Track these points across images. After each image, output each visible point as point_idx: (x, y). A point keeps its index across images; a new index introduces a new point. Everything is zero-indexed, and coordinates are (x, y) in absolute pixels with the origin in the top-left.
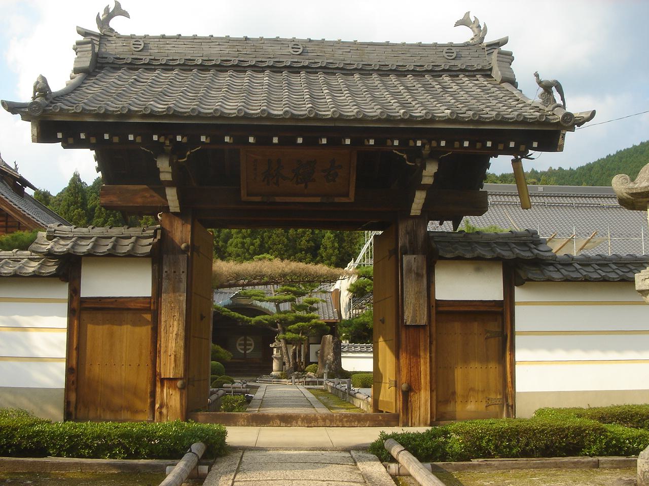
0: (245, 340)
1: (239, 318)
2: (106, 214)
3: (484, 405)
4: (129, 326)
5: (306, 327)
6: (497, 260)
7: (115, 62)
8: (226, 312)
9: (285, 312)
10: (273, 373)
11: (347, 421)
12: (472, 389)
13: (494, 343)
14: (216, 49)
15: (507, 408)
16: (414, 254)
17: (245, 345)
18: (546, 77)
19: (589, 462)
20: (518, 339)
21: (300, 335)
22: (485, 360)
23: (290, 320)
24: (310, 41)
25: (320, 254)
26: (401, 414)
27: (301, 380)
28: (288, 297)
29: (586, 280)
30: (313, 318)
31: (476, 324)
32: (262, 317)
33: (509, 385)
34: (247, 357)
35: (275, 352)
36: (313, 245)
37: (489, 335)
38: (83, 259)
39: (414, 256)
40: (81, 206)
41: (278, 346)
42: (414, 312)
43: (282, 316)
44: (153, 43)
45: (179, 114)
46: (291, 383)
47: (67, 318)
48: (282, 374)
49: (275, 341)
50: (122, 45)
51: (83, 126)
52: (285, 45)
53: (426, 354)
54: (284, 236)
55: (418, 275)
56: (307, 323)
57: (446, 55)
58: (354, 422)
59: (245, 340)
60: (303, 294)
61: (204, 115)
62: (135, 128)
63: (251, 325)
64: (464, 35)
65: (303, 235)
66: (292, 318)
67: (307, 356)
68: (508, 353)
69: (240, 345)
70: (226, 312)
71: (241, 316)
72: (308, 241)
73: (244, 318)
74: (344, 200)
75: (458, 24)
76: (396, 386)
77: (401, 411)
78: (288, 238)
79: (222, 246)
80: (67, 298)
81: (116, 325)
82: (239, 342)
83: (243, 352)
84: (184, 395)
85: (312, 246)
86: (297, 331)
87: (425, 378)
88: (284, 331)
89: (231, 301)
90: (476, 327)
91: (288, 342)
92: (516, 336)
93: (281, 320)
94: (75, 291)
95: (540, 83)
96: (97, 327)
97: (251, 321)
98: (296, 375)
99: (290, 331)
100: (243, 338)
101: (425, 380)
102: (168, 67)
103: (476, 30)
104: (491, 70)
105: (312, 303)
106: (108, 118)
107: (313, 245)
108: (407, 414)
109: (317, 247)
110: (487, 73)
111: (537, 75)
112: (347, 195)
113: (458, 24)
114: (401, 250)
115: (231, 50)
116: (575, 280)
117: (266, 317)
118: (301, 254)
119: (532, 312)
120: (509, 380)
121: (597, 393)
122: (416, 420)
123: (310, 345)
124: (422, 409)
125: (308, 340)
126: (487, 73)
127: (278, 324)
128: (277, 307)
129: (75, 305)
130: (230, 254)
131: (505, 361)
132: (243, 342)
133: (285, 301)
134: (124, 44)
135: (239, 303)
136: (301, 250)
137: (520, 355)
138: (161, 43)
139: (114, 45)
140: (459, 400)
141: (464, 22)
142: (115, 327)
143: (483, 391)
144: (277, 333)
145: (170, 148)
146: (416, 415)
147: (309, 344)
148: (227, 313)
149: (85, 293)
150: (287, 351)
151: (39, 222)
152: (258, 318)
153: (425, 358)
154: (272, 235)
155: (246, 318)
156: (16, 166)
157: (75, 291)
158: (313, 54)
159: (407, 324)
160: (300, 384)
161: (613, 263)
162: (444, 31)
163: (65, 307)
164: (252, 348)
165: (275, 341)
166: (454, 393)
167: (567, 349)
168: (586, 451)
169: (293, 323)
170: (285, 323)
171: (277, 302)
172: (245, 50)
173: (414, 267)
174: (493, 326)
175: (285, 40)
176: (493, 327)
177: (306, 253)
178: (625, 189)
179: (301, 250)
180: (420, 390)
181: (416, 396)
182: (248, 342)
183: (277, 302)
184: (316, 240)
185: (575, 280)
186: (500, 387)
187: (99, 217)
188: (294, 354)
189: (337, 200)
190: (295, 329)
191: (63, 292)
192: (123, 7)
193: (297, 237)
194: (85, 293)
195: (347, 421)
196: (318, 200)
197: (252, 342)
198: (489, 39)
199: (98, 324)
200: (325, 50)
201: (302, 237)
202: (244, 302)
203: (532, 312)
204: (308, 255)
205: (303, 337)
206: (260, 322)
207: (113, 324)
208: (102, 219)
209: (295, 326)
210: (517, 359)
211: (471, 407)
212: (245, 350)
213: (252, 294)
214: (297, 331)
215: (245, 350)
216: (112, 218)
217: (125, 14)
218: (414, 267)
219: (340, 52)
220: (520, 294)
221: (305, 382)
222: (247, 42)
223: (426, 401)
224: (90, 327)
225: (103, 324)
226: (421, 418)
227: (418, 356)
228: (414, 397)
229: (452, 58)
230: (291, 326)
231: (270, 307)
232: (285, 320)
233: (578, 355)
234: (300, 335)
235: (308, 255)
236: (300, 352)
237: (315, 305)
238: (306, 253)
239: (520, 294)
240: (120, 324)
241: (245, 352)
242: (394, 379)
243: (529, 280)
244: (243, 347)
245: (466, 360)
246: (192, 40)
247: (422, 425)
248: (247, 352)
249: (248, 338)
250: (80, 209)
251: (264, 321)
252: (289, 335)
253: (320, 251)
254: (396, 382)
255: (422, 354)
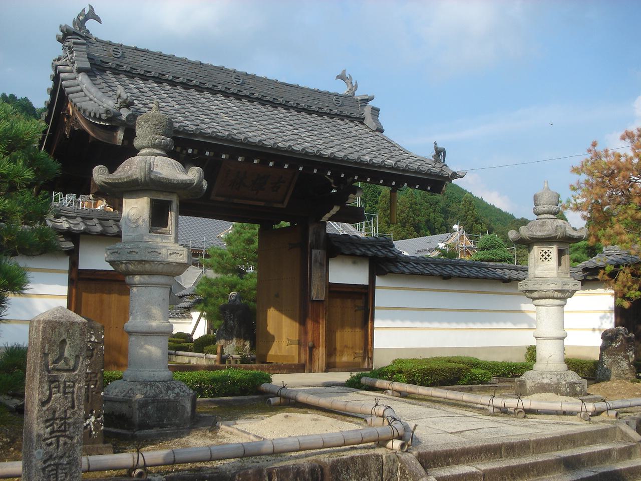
3: (353, 357)
4: (116, 295)
6: (363, 256)
7: (102, 65)
11: (272, 370)
12: (346, 346)
13: (359, 314)
14: (179, 68)
15: (368, 359)
16: (318, 249)
18: (439, 146)
19: (468, 388)
20: (376, 312)
22: (353, 326)
24: (247, 74)
26: (308, 364)
29: (485, 278)
31: (349, 301)
33: (370, 343)
37: (356, 308)
38: (81, 236)
39: (319, 251)
42: (317, 292)
44: (128, 52)
45: (234, 140)
47: (67, 287)
50: (102, 49)
51: (201, 147)
52: (229, 75)
53: (323, 321)
55: (321, 264)
57: (335, 102)
58: (277, 370)
61: (250, 144)
62: (224, 149)
64: (342, 89)
68: (370, 321)
74: (280, 206)
75: (339, 77)
76: (299, 344)
77: (308, 361)
80: (68, 269)
81: (106, 294)
87: (323, 338)
90: (349, 303)
92: (375, 310)
94: (74, 264)
95: (436, 149)
96: (90, 295)
101: (322, 340)
102: (131, 75)
103: (350, 86)
104: (364, 119)
106: (179, 135)
108: (311, 364)
110: (361, 120)
111: (435, 144)
112: (282, 202)
113: (339, 77)
114: (310, 246)
115: (190, 71)
116: (415, 274)
119: (386, 294)
120: (370, 340)
121: (418, 350)
122: (316, 368)
124: (320, 361)
126: (361, 120)
129: (74, 275)
131: (368, 327)
134: (104, 49)
137: (377, 323)
138: (135, 54)
139: (96, 48)
140: (338, 353)
141: (342, 77)
142: (105, 296)
143: (352, 348)
145: (184, 156)
146: (317, 364)
149: (82, 266)
153: (323, 324)
157: (74, 264)
158: (249, 86)
159: (314, 299)
161: (431, 263)
162: (321, 79)
163: (65, 277)
166: (335, 349)
167: (403, 319)
168: (461, 382)
172: (200, 73)
173: (319, 259)
174: (361, 303)
175: (228, 70)
176: (360, 303)
178: (529, 235)
180: (319, 346)
181: (317, 351)
185: (415, 274)
186: (362, 345)
189: (275, 205)
191: (65, 264)
192: (96, 12)
194: (82, 266)
195: (272, 370)
196: (262, 204)
198: (359, 94)
199: (91, 293)
200: (257, 83)
203: (386, 294)
207: (103, 292)
210: (375, 325)
211: (345, 359)
217: (98, 19)
218: (319, 259)
219: (267, 87)
220: (379, 282)
222: (201, 66)
223: (322, 355)
224: (84, 295)
225: (95, 293)
226: (320, 366)
227: (319, 323)
228: (315, 352)
229: (339, 105)
233: (408, 324)
239: (379, 282)
240: (110, 293)
242: (297, 338)
243: (391, 272)
245: (343, 326)
246: (160, 57)
247: (320, 371)
254: (299, 341)
255: (321, 321)
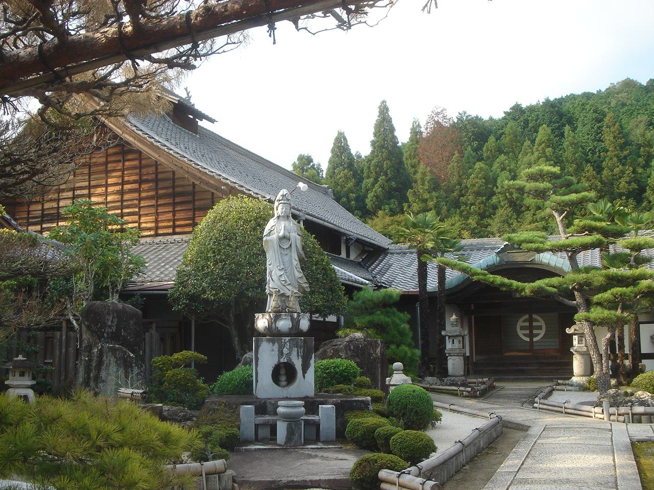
0: (531, 320)
1: (503, 285)
2: (376, 172)
5: (629, 296)
8: (478, 274)
9: (587, 270)
10: (574, 379)
17: (531, 328)
21: (619, 312)
23: (596, 284)
25: (646, 198)
27: (622, 410)
28: (588, 239)
30: (643, 277)
32: (547, 280)
34: (535, 348)
35: (575, 342)
36: (636, 187)
40: (348, 167)
41: (581, 331)
43: (582, 277)
46: (601, 416)
48: (590, 382)
49: (575, 323)
54: (596, 178)
56: (630, 289)
59: (531, 320)
60: (620, 234)
63: (526, 298)
65: (621, 175)
66: (601, 279)
67: (636, 345)
69: (522, 328)
70: (478, 274)
71: (506, 280)
72: (629, 183)
73: (511, 285)
78: (601, 181)
79: (517, 198)
82: (520, 323)
83: (528, 339)
84: (503, 377)
85: (635, 188)
86: (612, 305)
88: (588, 304)
89: (498, 258)
91: (593, 323)
93: (579, 284)
97: (523, 289)
98: (613, 396)
99: (599, 304)
100: (527, 316)
105: (637, 248)
107: (636, 187)
109: (642, 190)
117: (555, 280)
118: (621, 199)
123: (640, 325)
125: (637, 318)
127: (576, 293)
128: (572, 259)
130: (528, 207)
132: (527, 324)
133: (585, 247)
135: (511, 260)
136: (620, 195)
144: (575, 310)
147: (638, 324)
148: (481, 277)
150: (595, 341)
151: (171, 152)
152: (539, 283)
154: (581, 179)
155: (515, 283)
156: (188, 94)
160: (621, 418)
164: (542, 333)
165: (575, 323)
169: (603, 289)
170: (587, 290)
171: (573, 251)
177: (627, 198)
179: (620, 195)
182: (535, 324)
183: (573, 251)
184: (639, 181)
187: (368, 177)
188: (611, 343)
190: (609, 301)
193: (614, 179)
197: (542, 323)
201: (620, 178)
202: (519, 257)
204: (631, 201)
205: (625, 314)
206: (540, 291)
208: (372, 179)
209: (607, 295)
212: (531, 336)
213: (522, 239)
214: (612, 305)
215: (531, 336)
216: (384, 177)
221: (633, 414)
230: (600, 295)
231: (559, 261)
232: (588, 283)
234: (619, 312)
235: (631, 201)
236: (621, 339)
237: (644, 253)
238: (627, 198)
241: (531, 340)
244: (527, 332)
248: (535, 339)
249: (534, 316)
250: (346, 171)
251: (548, 288)
252: (597, 313)
253: (647, 194)
